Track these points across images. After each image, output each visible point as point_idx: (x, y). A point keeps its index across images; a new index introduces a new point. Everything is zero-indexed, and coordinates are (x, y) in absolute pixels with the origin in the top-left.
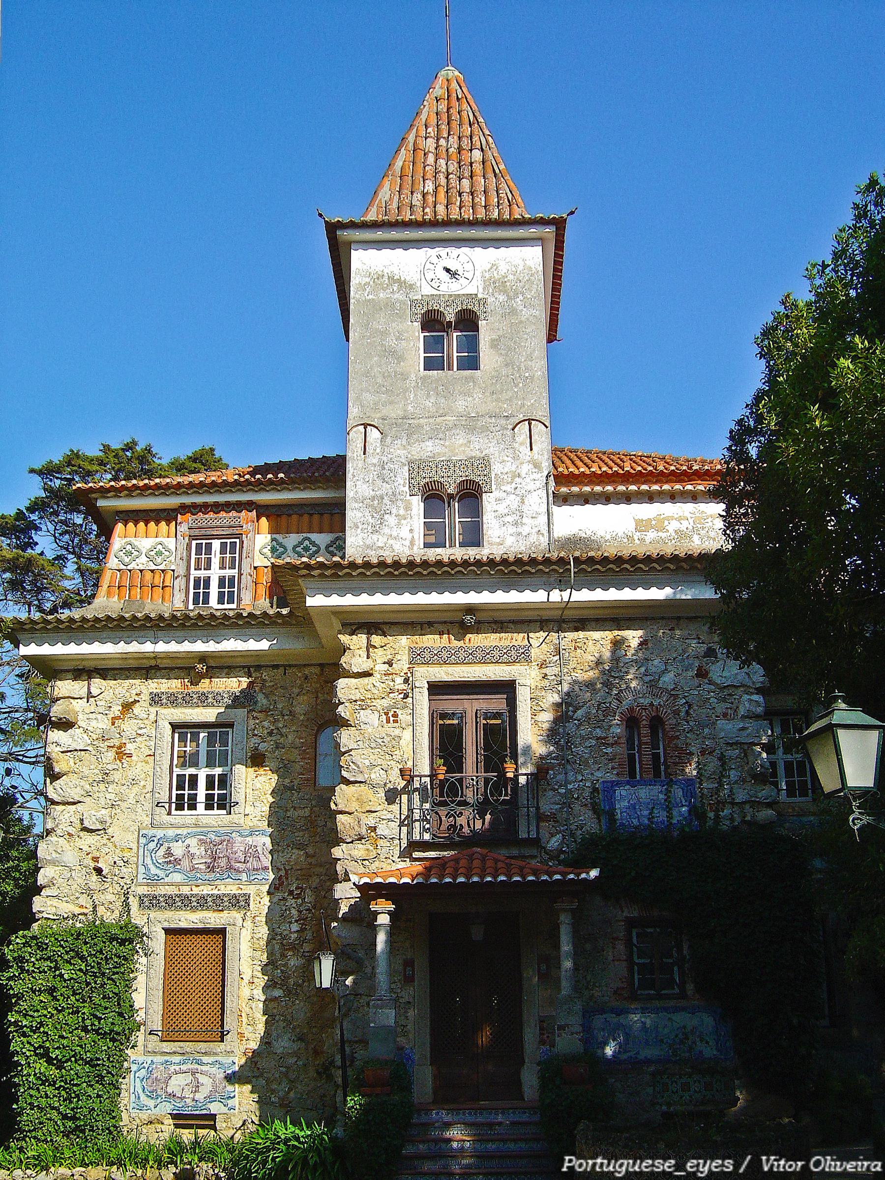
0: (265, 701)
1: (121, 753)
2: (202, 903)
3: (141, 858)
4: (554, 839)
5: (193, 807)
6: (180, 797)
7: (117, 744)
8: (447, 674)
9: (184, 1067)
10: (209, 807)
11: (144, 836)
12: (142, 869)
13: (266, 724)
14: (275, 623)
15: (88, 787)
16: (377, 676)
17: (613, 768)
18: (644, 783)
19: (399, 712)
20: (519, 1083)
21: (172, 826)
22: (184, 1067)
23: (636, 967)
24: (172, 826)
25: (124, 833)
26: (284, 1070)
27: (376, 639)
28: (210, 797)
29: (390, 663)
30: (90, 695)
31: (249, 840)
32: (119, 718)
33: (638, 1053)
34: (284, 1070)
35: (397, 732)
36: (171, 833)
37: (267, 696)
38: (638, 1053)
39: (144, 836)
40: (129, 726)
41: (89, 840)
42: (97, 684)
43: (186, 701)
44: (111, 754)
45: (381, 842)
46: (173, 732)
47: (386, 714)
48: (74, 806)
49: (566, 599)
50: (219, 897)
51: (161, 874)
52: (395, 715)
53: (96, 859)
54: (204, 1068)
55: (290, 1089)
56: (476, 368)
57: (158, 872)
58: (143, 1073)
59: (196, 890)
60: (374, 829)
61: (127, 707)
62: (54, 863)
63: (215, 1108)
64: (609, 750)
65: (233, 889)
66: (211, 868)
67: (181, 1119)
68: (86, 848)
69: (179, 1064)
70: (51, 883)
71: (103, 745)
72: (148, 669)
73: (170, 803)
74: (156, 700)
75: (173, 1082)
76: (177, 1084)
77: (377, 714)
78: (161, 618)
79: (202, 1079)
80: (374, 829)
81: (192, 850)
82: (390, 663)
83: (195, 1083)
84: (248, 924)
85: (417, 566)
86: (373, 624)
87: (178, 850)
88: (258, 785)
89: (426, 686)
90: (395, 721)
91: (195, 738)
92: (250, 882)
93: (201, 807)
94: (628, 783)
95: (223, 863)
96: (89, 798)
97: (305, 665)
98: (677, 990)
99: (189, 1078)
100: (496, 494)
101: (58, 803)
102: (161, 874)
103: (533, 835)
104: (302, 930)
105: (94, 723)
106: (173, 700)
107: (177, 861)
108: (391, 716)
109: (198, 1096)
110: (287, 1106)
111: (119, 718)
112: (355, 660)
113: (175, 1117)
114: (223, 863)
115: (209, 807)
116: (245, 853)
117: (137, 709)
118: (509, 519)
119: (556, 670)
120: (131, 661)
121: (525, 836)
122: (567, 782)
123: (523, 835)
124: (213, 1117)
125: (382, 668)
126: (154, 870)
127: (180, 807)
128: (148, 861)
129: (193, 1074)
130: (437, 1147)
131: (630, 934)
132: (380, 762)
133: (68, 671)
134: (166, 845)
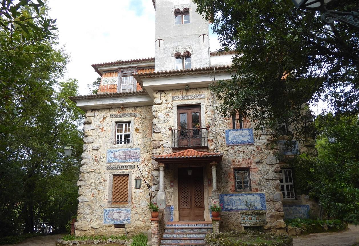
0: (139, 115)
1: (103, 130)
2: (123, 167)
3: (107, 156)
4: (212, 146)
5: (121, 143)
6: (118, 141)
7: (102, 128)
8: (182, 103)
9: (117, 211)
10: (125, 143)
11: (108, 151)
12: (107, 159)
13: (139, 121)
14: (140, 94)
15: (94, 139)
16: (163, 104)
17: (228, 126)
18: (238, 130)
19: (169, 113)
20: (203, 216)
21: (115, 148)
22: (117, 211)
23: (237, 182)
24: (115, 148)
25: (103, 150)
26: (143, 211)
27: (163, 95)
28: (125, 140)
29: (167, 101)
30: (95, 116)
31: (135, 151)
32: (102, 121)
33: (238, 207)
34: (143, 211)
35: (168, 119)
36: (115, 150)
37: (139, 114)
38: (238, 207)
39: (108, 151)
40: (105, 123)
41: (94, 153)
42: (97, 113)
43: (119, 116)
44: (100, 130)
45: (164, 148)
46: (116, 124)
47: (166, 114)
48: (91, 144)
49: (213, 80)
50: (127, 166)
51: (112, 160)
52: (168, 114)
53: (96, 157)
54: (123, 211)
55: (145, 217)
56: (189, 23)
57: (111, 160)
58: (107, 213)
59: (121, 164)
60: (162, 145)
61: (104, 118)
62: (86, 158)
63: (125, 222)
64: (227, 121)
65: (131, 164)
66: (125, 158)
67: (117, 226)
68: (93, 154)
69: (116, 210)
70: (85, 163)
71: (98, 128)
72: (109, 108)
73: (115, 142)
74: (111, 116)
75: (114, 215)
76: (116, 216)
77: (163, 114)
78: (111, 94)
79: (122, 214)
80: (162, 145)
81: (120, 154)
82: (167, 101)
83: (120, 215)
84: (134, 173)
85: (172, 73)
86: (162, 90)
87: (117, 154)
88: (137, 137)
89: (176, 106)
90: (168, 116)
91: (122, 125)
92: (135, 162)
93: (123, 143)
94: (233, 130)
95: (128, 157)
96: (94, 142)
97: (149, 106)
98: (249, 189)
99: (118, 214)
100: (195, 54)
101: (87, 143)
102: (112, 160)
103: (206, 145)
104: (148, 174)
105: (96, 123)
106: (116, 116)
107: (116, 157)
108: (167, 114)
109: (121, 219)
110: (144, 221)
111: (102, 121)
112: (158, 100)
113: (114, 225)
114: (128, 157)
115: (125, 143)
116: (134, 154)
117: (107, 119)
118: (198, 61)
119: (212, 100)
120: (105, 107)
121: (204, 145)
122: (215, 130)
123: (203, 145)
124: (124, 225)
125: (164, 102)
126: (110, 159)
127: (118, 143)
128: (109, 157)
129: (120, 213)
130: (176, 236)
131: (235, 173)
132: (164, 127)
133: (89, 110)
134: (114, 153)
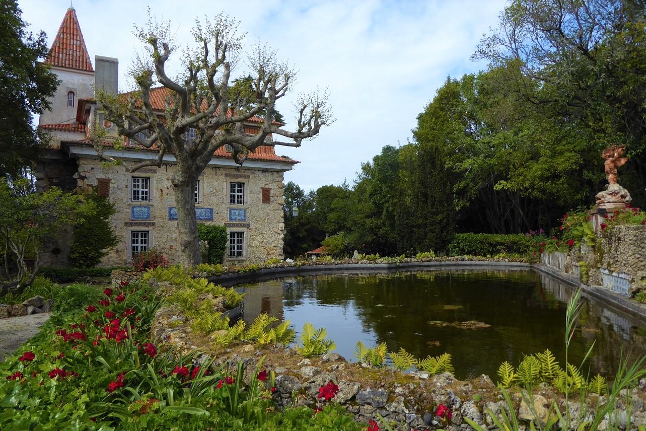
93: (140, 200)
